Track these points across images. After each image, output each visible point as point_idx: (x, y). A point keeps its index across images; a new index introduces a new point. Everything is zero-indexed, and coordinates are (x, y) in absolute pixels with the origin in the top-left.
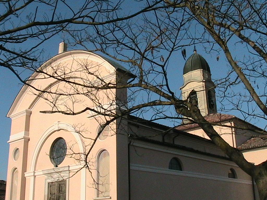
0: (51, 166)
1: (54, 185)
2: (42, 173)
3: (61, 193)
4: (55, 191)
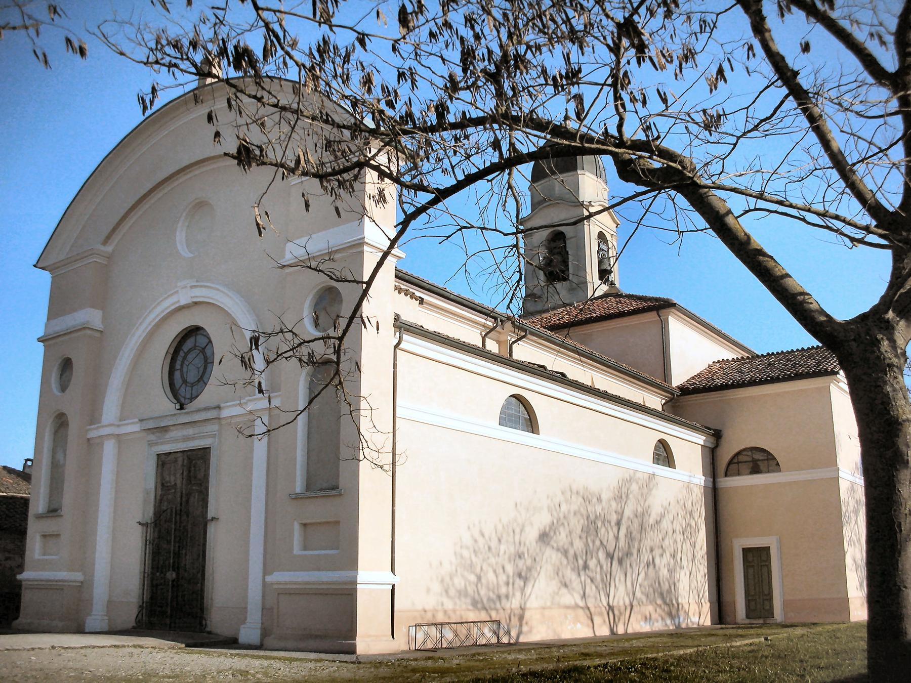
0: (165, 405)
1: (176, 461)
2: (136, 428)
3: (193, 482)
4: (177, 479)
